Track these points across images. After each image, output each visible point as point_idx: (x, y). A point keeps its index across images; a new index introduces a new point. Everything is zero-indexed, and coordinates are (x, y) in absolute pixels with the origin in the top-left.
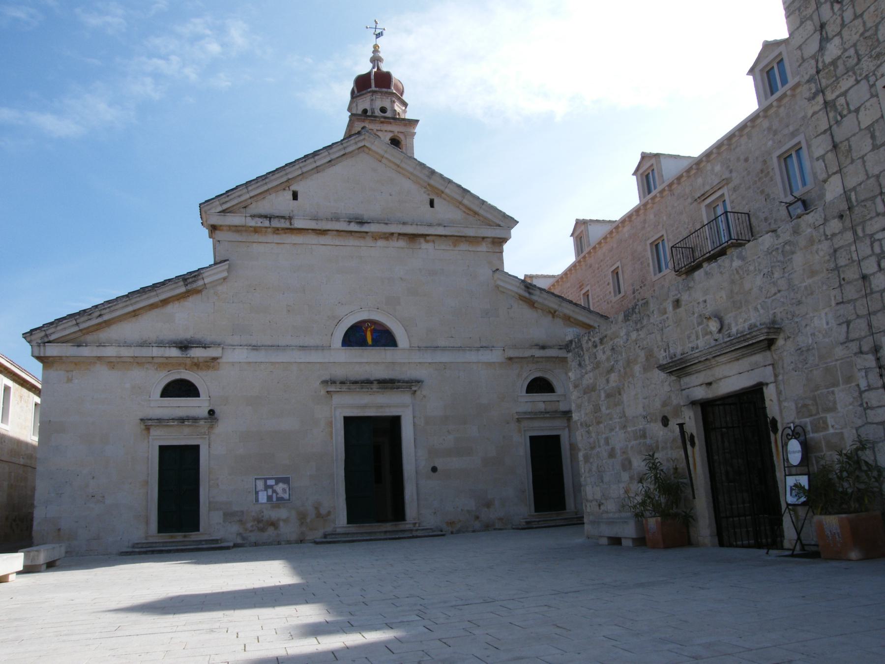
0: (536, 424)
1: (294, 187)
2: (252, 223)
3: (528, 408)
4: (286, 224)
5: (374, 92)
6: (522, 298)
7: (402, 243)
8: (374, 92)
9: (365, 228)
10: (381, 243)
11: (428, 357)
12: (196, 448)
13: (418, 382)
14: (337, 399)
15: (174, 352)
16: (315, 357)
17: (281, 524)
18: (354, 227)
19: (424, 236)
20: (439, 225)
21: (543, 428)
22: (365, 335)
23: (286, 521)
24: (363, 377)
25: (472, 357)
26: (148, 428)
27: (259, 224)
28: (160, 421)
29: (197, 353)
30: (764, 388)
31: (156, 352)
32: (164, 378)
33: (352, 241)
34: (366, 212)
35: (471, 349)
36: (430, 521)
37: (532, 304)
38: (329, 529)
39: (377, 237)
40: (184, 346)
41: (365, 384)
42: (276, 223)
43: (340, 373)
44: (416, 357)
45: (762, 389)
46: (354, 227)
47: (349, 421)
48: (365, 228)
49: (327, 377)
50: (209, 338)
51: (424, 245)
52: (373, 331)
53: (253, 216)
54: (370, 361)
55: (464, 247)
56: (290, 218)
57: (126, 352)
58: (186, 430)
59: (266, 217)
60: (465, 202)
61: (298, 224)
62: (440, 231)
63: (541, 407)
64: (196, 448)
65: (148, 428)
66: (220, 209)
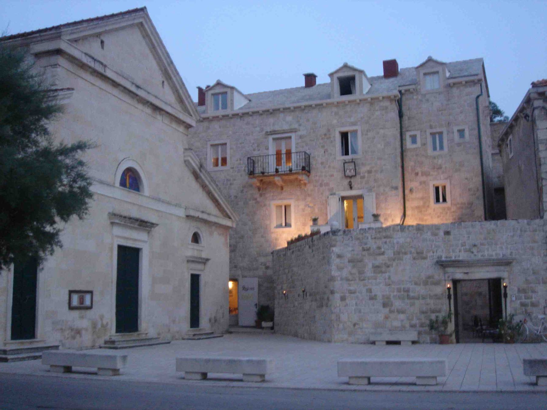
7: (149, 111)
10: (140, 106)
14: (117, 231)
17: (83, 332)
21: (196, 269)
23: (86, 330)
24: (135, 214)
27: (89, 64)
36: (152, 333)
37: (197, 177)
38: (107, 338)
49: (111, 211)
51: (159, 117)
52: (130, 177)
53: (86, 54)
55: (174, 125)
56: (105, 66)
59: (93, 58)
60: (181, 92)
63: (196, 254)
66: (69, 37)
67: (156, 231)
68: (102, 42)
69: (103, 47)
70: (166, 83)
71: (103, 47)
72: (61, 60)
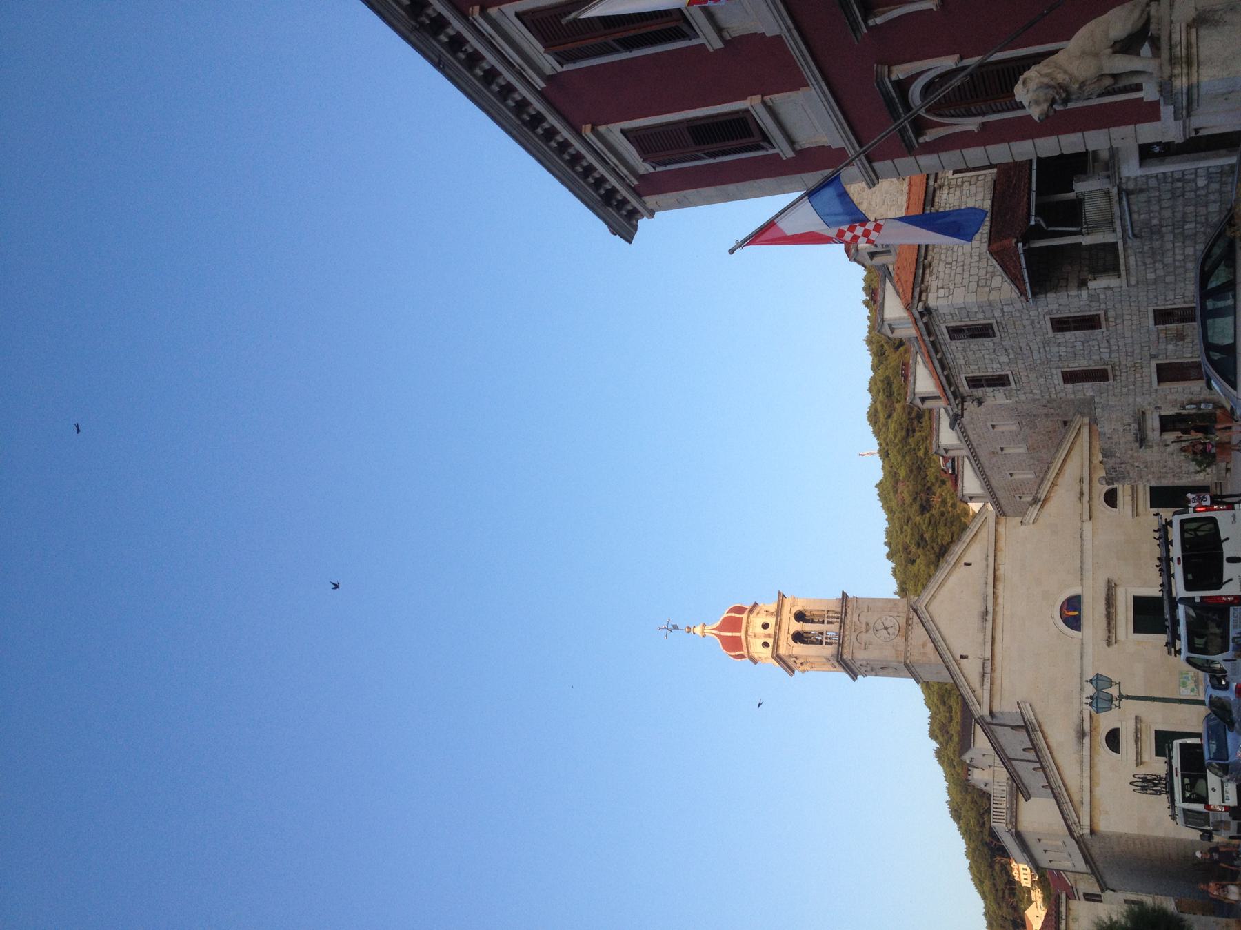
0: (1141, 502)
1: (958, 657)
2: (987, 685)
3: (1128, 510)
4: (988, 664)
5: (747, 634)
6: (1042, 507)
7: (1000, 586)
8: (747, 634)
9: (990, 609)
10: (1000, 600)
11: (1089, 574)
12: (1157, 732)
13: (1109, 582)
15: (1087, 741)
16: (1089, 650)
18: (990, 618)
19: (995, 571)
20: (987, 560)
22: (1072, 613)
25: (1088, 546)
26: (1142, 763)
28: (1139, 753)
29: (1087, 726)
30: (1163, 638)
31: (1086, 753)
32: (1104, 750)
33: (999, 621)
34: (977, 608)
35: (1082, 545)
37: (1046, 499)
39: (995, 604)
40: (1082, 734)
41: (1110, 617)
42: (988, 670)
43: (1102, 633)
44: (1088, 582)
45: (1160, 630)
46: (990, 618)
47: (1137, 630)
48: (990, 609)
49: (1105, 643)
50: (1077, 720)
54: (1093, 612)
55: (1001, 544)
57: (1087, 773)
58: (1144, 737)
61: (988, 655)
62: (991, 560)
63: (1128, 499)
64: (1157, 732)
65: (1142, 763)
67: (1115, 578)
68: (962, 657)
69: (966, 657)
70: (966, 560)
71: (966, 657)
72: (995, 710)
